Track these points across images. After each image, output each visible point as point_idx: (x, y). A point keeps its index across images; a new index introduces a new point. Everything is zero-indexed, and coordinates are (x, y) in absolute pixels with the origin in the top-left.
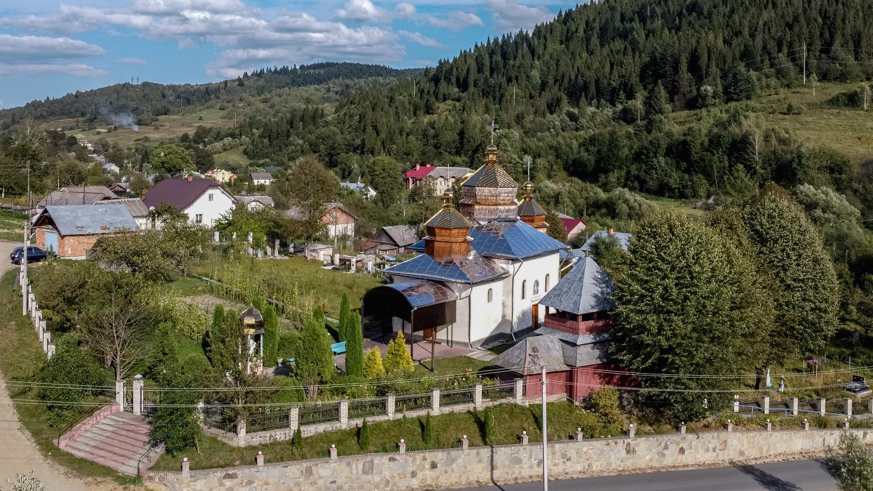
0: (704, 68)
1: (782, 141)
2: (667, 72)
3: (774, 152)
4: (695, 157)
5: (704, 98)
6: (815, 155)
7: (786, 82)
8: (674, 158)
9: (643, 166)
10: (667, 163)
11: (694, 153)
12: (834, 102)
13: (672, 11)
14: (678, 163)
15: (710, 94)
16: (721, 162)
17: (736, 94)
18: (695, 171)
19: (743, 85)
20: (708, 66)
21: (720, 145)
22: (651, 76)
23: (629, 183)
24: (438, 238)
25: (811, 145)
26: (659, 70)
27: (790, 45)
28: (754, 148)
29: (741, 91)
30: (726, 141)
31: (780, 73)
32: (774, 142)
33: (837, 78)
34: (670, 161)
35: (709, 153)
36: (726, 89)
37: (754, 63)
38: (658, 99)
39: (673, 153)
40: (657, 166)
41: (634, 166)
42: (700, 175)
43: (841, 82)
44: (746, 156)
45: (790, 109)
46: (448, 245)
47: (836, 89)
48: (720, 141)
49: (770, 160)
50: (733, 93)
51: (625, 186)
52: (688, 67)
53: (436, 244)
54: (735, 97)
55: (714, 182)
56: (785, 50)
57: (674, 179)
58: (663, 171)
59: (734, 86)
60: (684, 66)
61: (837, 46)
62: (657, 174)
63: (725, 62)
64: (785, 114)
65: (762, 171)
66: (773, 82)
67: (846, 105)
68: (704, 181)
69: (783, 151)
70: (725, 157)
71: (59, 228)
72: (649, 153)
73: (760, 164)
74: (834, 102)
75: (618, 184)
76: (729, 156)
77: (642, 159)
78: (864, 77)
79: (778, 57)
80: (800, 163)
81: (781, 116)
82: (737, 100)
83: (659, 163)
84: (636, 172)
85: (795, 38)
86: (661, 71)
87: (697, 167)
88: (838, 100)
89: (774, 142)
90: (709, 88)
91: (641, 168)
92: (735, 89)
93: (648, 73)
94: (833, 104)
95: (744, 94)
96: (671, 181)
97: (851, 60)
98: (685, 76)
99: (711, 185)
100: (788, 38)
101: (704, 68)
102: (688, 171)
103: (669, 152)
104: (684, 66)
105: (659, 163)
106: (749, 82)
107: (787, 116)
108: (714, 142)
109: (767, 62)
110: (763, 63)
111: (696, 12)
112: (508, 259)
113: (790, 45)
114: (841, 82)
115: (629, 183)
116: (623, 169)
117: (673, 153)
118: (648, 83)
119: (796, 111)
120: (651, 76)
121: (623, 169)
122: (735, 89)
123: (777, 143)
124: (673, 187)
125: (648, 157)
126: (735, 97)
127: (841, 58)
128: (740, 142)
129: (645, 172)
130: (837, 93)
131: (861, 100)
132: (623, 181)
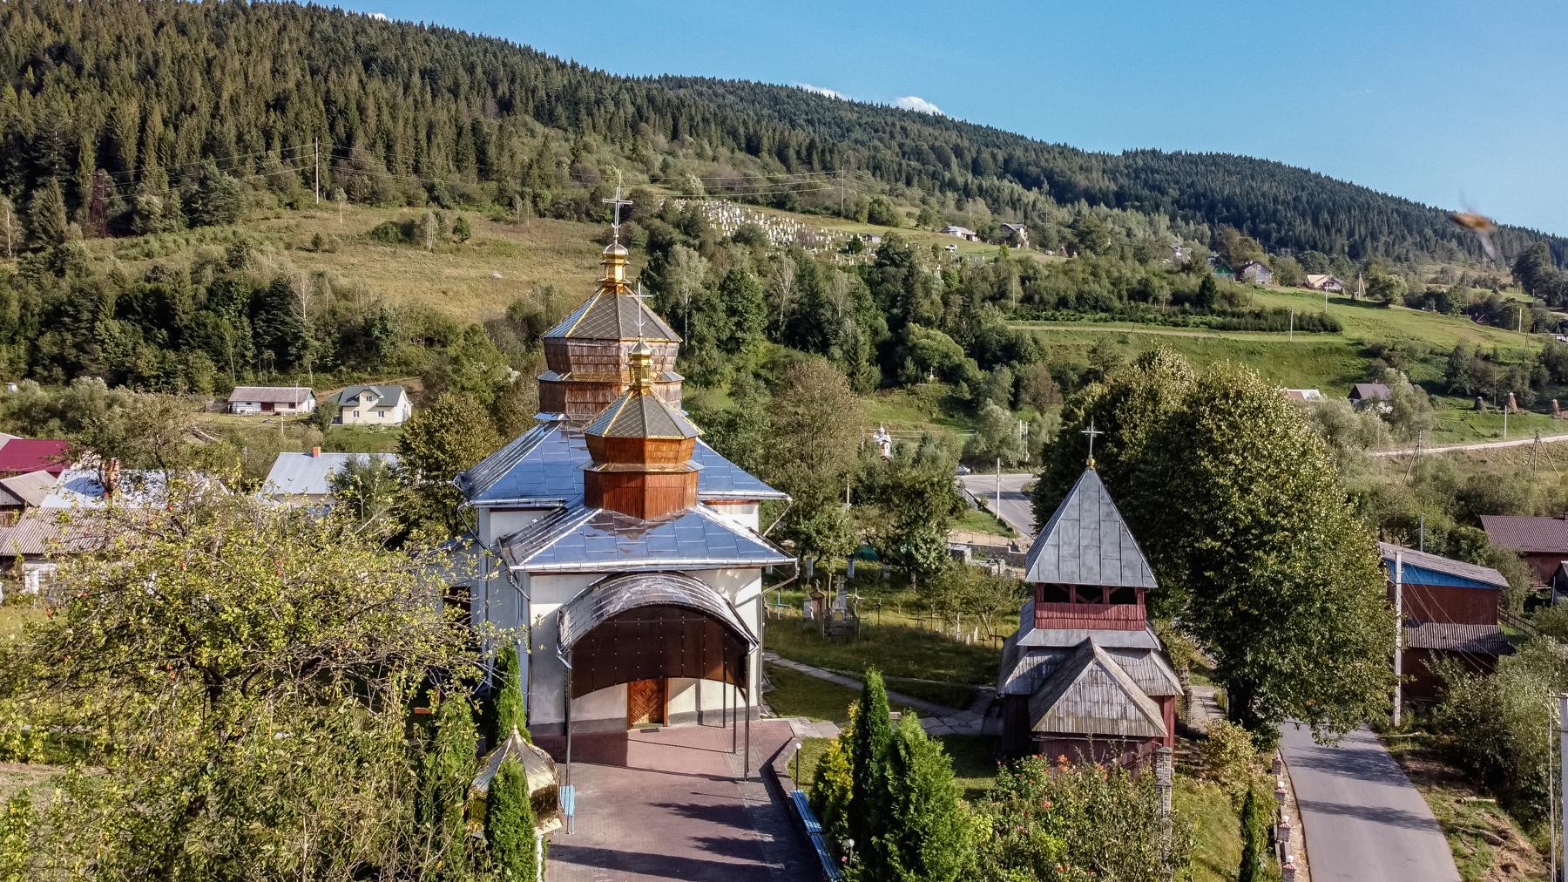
0: (131, 164)
1: (344, 295)
2: (53, 164)
3: (333, 313)
4: (183, 319)
5: (146, 217)
6: (412, 315)
7: (286, 200)
8: (140, 322)
9: (68, 336)
10: (123, 331)
11: (180, 313)
12: (379, 234)
13: (13, 54)
14: (146, 330)
15: (158, 210)
16: (236, 328)
17: (208, 212)
18: (188, 344)
19: (218, 199)
20: (140, 162)
21: (231, 299)
22: (19, 169)
23: (39, 370)
24: (650, 467)
25: (398, 302)
26: (37, 159)
27: (285, 139)
28: (298, 302)
29: (217, 208)
30: (243, 293)
31: (274, 184)
32: (328, 294)
33: (365, 199)
34: (129, 328)
35: (211, 314)
36: (187, 202)
37: (229, 163)
38: (53, 214)
39: (135, 312)
40: (105, 336)
41: (48, 337)
42: (199, 352)
43: (371, 204)
44: (288, 319)
45: (317, 242)
46: (675, 481)
47: (375, 217)
48: (230, 292)
49: (326, 324)
50: (203, 211)
51: (31, 374)
52: (97, 159)
53: (650, 481)
54: (206, 217)
55: (227, 363)
56: (277, 144)
57: (147, 358)
58: (117, 345)
59: (202, 198)
60: (89, 157)
61: (359, 147)
62: (104, 350)
63: (174, 156)
64: (310, 251)
65: (317, 344)
66: (268, 198)
67: (400, 241)
68: (208, 363)
69: (347, 309)
70: (244, 318)
71: (659, 808)
72: (79, 312)
73: (312, 332)
74: (379, 234)
75: (13, 373)
76: (251, 317)
77: (65, 325)
78: (403, 199)
79: (268, 157)
80: (384, 330)
81: (304, 254)
82: (209, 224)
83: (107, 330)
84: (55, 350)
85: (290, 127)
86: (43, 162)
87: (192, 337)
88: (387, 233)
89: (328, 294)
90: (155, 200)
91: (64, 341)
92: (205, 205)
93: (10, 163)
94: (379, 238)
95: (221, 214)
96: (141, 363)
97: (383, 174)
98: (91, 177)
99: (221, 369)
100: (280, 126)
101: (131, 164)
102: (173, 343)
103: (123, 310)
104: (89, 157)
105: (107, 330)
106: (230, 193)
107: (312, 254)
108: (219, 294)
109: (250, 163)
110: (243, 164)
111: (68, 62)
112: (751, 502)
113: (285, 139)
114: (371, 204)
115: (39, 370)
116: (19, 343)
117: (135, 312)
118: (12, 182)
119: (327, 247)
120: (19, 169)
121: (19, 343)
122: (205, 205)
123: (333, 297)
124: (146, 374)
125: (76, 319)
126: (206, 217)
127: (368, 167)
128: (271, 294)
129: (76, 346)
130: (383, 221)
131: (423, 235)
132: (23, 365)
